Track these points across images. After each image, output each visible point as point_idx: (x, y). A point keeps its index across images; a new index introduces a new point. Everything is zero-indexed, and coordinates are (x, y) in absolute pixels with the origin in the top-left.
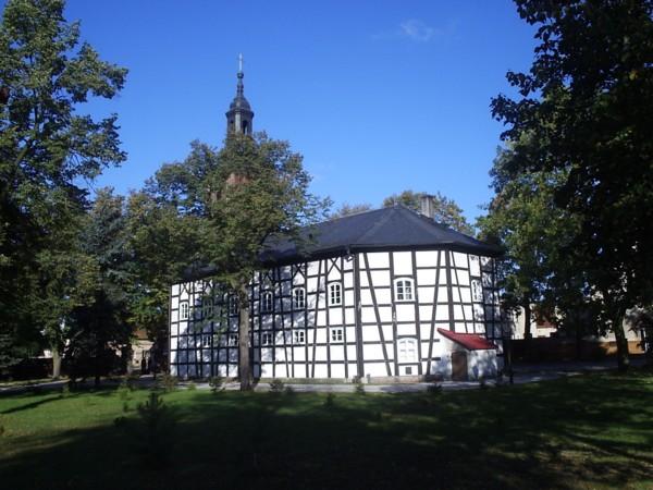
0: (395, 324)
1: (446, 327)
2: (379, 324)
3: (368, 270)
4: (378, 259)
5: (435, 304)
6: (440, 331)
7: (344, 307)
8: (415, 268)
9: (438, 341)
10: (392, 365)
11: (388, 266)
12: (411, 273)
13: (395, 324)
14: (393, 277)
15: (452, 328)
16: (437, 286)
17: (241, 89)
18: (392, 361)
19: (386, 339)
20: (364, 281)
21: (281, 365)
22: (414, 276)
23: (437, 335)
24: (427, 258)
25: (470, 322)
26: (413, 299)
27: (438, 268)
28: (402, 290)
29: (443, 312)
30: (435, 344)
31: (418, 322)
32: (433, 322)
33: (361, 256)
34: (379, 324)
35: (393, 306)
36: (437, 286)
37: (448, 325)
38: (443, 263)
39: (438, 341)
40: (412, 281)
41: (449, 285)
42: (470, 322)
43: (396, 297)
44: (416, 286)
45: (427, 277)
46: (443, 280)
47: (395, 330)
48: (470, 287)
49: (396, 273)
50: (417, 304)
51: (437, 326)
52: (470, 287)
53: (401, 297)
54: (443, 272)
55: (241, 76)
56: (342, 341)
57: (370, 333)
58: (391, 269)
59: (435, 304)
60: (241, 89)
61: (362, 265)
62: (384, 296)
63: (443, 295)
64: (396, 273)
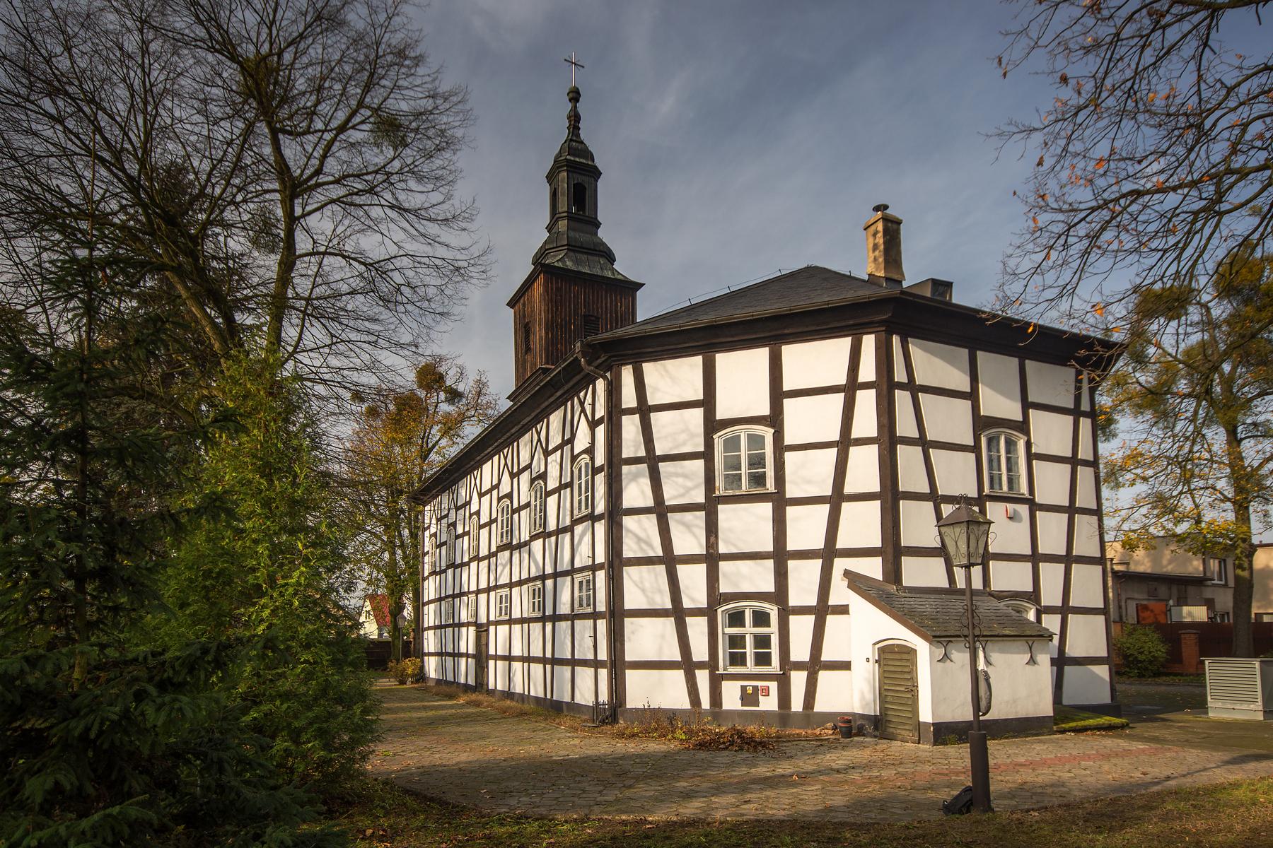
0: (712, 559)
1: (873, 568)
2: (670, 560)
3: (644, 410)
4: (673, 378)
5: (837, 498)
6: (856, 582)
7: (934, 497)
8: (778, 394)
9: (843, 610)
10: (702, 677)
11: (788, 456)
12: (765, 410)
13: (712, 559)
14: (712, 425)
15: (893, 573)
16: (845, 442)
17: (575, 119)
18: (701, 665)
19: (687, 603)
20: (632, 442)
21: (1086, 518)
22: (775, 419)
23: (840, 593)
24: (817, 361)
25: (584, 663)
26: (770, 486)
27: (851, 388)
28: (746, 466)
29: (863, 524)
30: (831, 620)
31: (781, 556)
32: (829, 553)
33: (627, 374)
34: (670, 560)
35: (710, 507)
36: (845, 442)
37: (599, 622)
38: (868, 372)
39: (843, 610)
40: (768, 433)
41: (888, 440)
42: (584, 663)
43: (720, 482)
44: (780, 448)
45: (811, 420)
46: (866, 421)
47: (713, 578)
48: (976, 449)
49: (721, 414)
50: (780, 502)
51: (840, 565)
52: (976, 449)
53: (734, 480)
54: (866, 402)
55: (575, 96)
56: (590, 610)
57: (643, 587)
58: (708, 402)
59: (837, 498)
60: (575, 119)
61: (629, 398)
62: (683, 484)
63: (864, 469)
64: (721, 414)
